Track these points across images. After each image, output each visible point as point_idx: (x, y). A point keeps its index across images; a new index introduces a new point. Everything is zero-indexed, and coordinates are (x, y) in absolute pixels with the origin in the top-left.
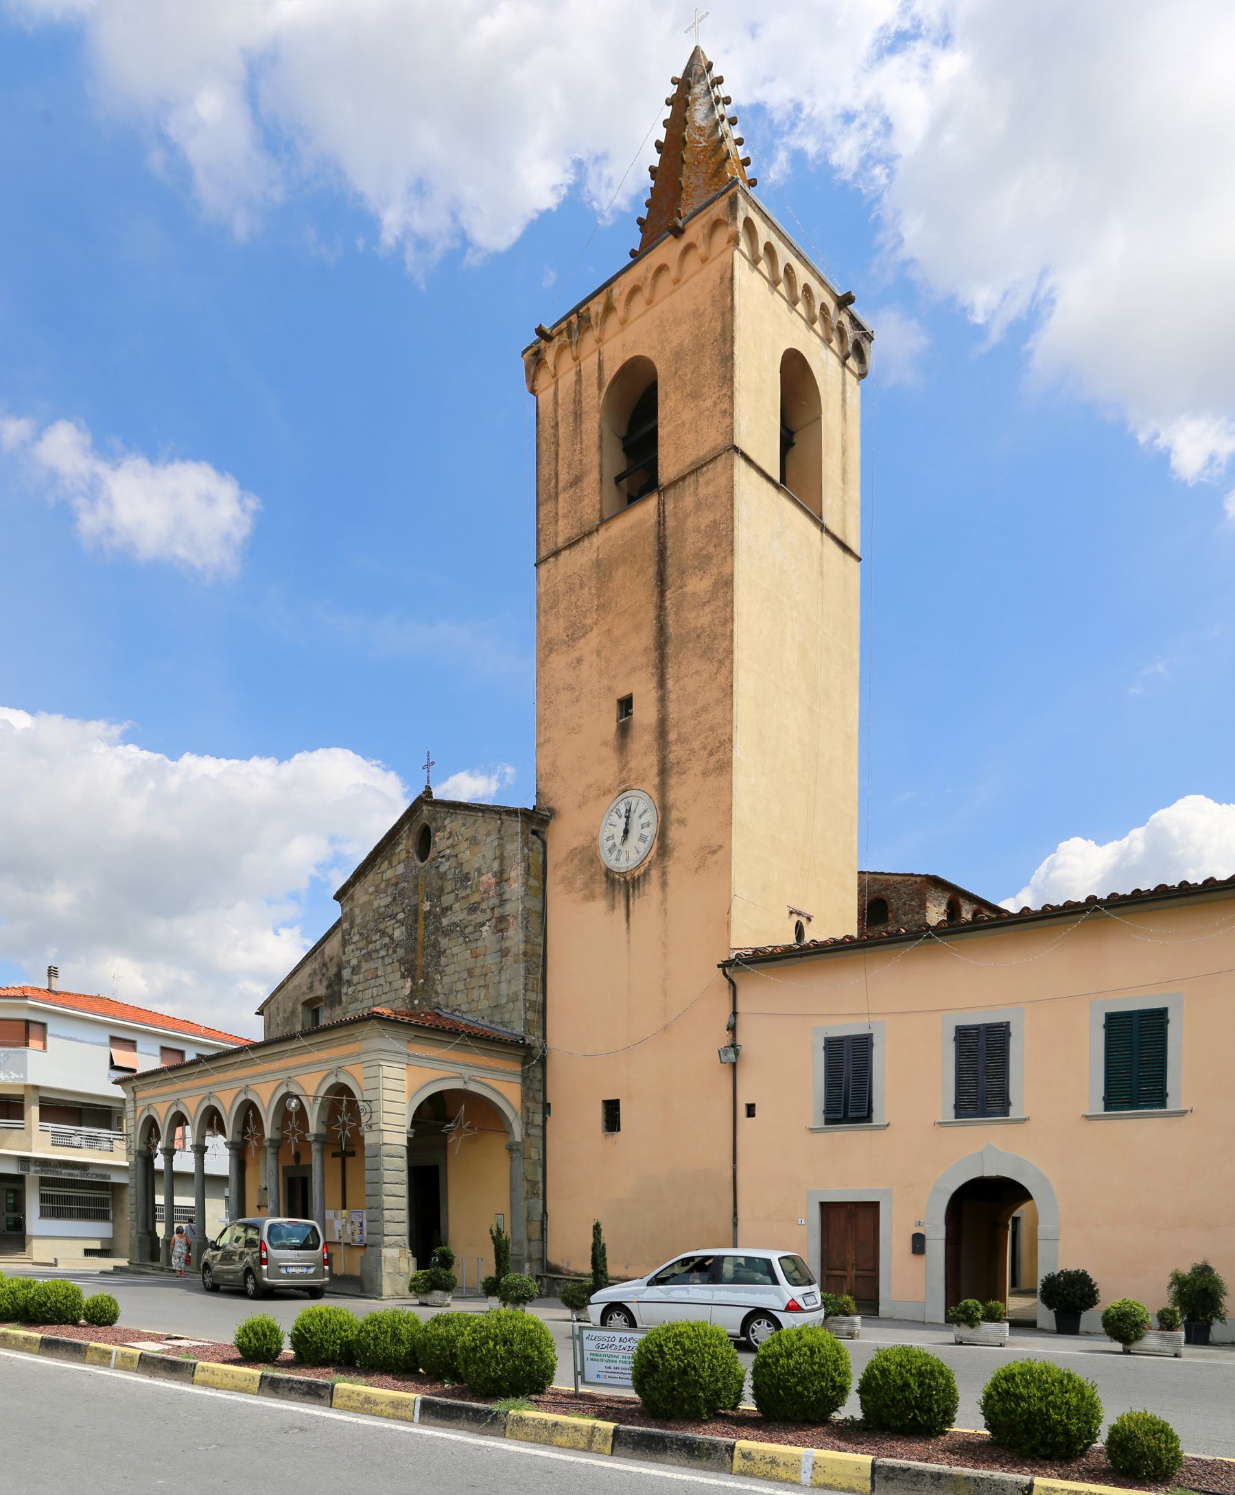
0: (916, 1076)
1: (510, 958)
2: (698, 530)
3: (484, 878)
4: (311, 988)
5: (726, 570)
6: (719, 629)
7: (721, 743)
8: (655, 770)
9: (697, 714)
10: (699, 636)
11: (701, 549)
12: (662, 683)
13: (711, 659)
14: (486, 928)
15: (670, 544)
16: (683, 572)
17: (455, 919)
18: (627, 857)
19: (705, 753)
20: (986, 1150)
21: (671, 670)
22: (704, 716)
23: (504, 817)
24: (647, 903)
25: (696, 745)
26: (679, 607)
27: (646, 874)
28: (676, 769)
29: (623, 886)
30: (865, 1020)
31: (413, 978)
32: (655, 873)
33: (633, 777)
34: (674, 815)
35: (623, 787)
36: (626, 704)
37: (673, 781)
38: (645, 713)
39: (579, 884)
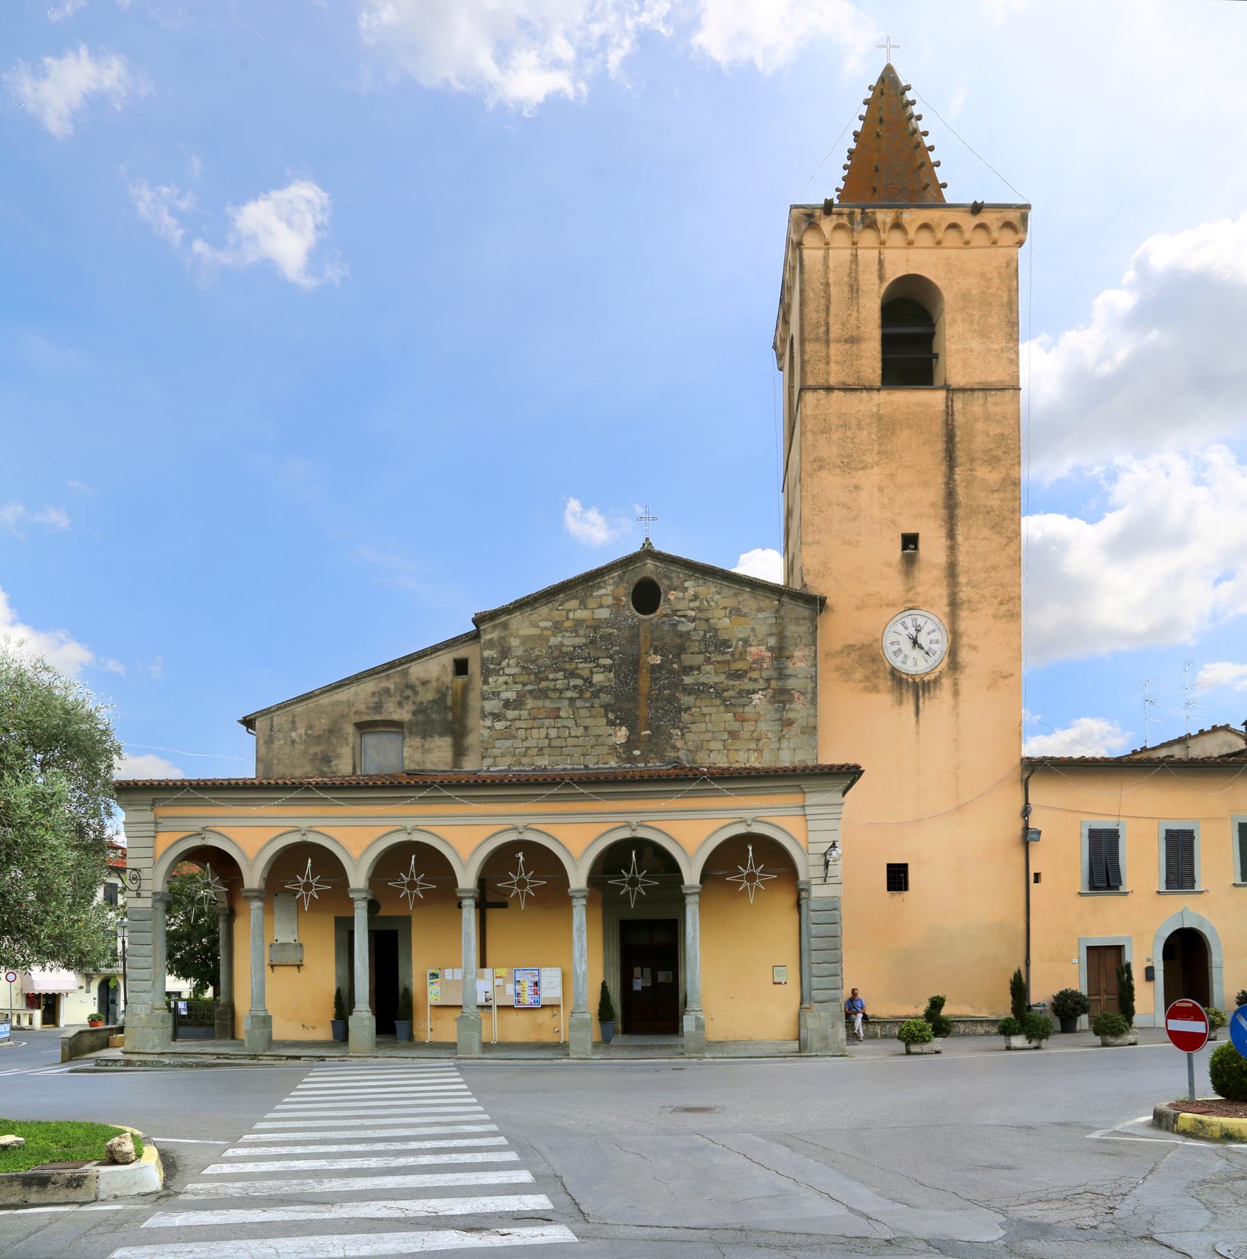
0: (1142, 862)
1: (795, 729)
2: (987, 434)
3: (753, 649)
4: (378, 707)
5: (1014, 474)
6: (1008, 514)
7: (1011, 599)
8: (945, 601)
9: (987, 570)
10: (988, 513)
11: (990, 450)
12: (951, 535)
13: (1001, 534)
14: (757, 696)
15: (958, 433)
16: (973, 460)
17: (702, 679)
18: (915, 664)
19: (996, 602)
20: (1182, 911)
21: (961, 530)
22: (993, 574)
23: (785, 599)
24: (937, 706)
25: (987, 592)
26: (969, 484)
27: (936, 681)
28: (966, 606)
29: (915, 689)
30: (1115, 819)
31: (632, 729)
32: (946, 682)
33: (920, 599)
34: (964, 640)
35: (910, 605)
36: (910, 541)
37: (964, 613)
38: (932, 549)
39: (858, 675)
